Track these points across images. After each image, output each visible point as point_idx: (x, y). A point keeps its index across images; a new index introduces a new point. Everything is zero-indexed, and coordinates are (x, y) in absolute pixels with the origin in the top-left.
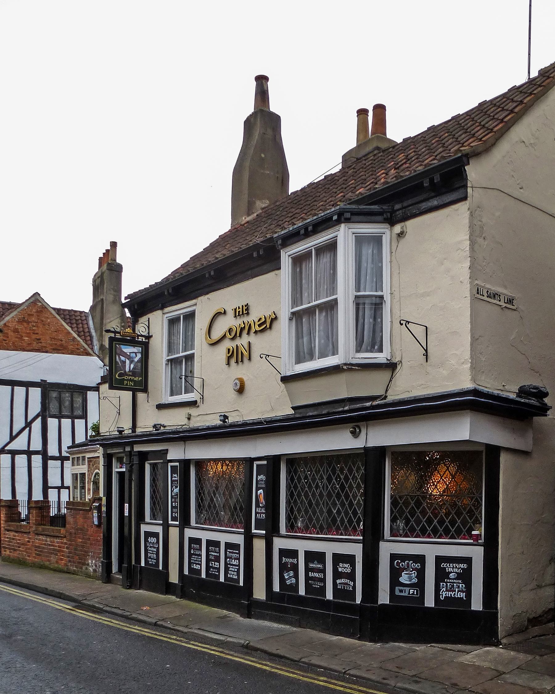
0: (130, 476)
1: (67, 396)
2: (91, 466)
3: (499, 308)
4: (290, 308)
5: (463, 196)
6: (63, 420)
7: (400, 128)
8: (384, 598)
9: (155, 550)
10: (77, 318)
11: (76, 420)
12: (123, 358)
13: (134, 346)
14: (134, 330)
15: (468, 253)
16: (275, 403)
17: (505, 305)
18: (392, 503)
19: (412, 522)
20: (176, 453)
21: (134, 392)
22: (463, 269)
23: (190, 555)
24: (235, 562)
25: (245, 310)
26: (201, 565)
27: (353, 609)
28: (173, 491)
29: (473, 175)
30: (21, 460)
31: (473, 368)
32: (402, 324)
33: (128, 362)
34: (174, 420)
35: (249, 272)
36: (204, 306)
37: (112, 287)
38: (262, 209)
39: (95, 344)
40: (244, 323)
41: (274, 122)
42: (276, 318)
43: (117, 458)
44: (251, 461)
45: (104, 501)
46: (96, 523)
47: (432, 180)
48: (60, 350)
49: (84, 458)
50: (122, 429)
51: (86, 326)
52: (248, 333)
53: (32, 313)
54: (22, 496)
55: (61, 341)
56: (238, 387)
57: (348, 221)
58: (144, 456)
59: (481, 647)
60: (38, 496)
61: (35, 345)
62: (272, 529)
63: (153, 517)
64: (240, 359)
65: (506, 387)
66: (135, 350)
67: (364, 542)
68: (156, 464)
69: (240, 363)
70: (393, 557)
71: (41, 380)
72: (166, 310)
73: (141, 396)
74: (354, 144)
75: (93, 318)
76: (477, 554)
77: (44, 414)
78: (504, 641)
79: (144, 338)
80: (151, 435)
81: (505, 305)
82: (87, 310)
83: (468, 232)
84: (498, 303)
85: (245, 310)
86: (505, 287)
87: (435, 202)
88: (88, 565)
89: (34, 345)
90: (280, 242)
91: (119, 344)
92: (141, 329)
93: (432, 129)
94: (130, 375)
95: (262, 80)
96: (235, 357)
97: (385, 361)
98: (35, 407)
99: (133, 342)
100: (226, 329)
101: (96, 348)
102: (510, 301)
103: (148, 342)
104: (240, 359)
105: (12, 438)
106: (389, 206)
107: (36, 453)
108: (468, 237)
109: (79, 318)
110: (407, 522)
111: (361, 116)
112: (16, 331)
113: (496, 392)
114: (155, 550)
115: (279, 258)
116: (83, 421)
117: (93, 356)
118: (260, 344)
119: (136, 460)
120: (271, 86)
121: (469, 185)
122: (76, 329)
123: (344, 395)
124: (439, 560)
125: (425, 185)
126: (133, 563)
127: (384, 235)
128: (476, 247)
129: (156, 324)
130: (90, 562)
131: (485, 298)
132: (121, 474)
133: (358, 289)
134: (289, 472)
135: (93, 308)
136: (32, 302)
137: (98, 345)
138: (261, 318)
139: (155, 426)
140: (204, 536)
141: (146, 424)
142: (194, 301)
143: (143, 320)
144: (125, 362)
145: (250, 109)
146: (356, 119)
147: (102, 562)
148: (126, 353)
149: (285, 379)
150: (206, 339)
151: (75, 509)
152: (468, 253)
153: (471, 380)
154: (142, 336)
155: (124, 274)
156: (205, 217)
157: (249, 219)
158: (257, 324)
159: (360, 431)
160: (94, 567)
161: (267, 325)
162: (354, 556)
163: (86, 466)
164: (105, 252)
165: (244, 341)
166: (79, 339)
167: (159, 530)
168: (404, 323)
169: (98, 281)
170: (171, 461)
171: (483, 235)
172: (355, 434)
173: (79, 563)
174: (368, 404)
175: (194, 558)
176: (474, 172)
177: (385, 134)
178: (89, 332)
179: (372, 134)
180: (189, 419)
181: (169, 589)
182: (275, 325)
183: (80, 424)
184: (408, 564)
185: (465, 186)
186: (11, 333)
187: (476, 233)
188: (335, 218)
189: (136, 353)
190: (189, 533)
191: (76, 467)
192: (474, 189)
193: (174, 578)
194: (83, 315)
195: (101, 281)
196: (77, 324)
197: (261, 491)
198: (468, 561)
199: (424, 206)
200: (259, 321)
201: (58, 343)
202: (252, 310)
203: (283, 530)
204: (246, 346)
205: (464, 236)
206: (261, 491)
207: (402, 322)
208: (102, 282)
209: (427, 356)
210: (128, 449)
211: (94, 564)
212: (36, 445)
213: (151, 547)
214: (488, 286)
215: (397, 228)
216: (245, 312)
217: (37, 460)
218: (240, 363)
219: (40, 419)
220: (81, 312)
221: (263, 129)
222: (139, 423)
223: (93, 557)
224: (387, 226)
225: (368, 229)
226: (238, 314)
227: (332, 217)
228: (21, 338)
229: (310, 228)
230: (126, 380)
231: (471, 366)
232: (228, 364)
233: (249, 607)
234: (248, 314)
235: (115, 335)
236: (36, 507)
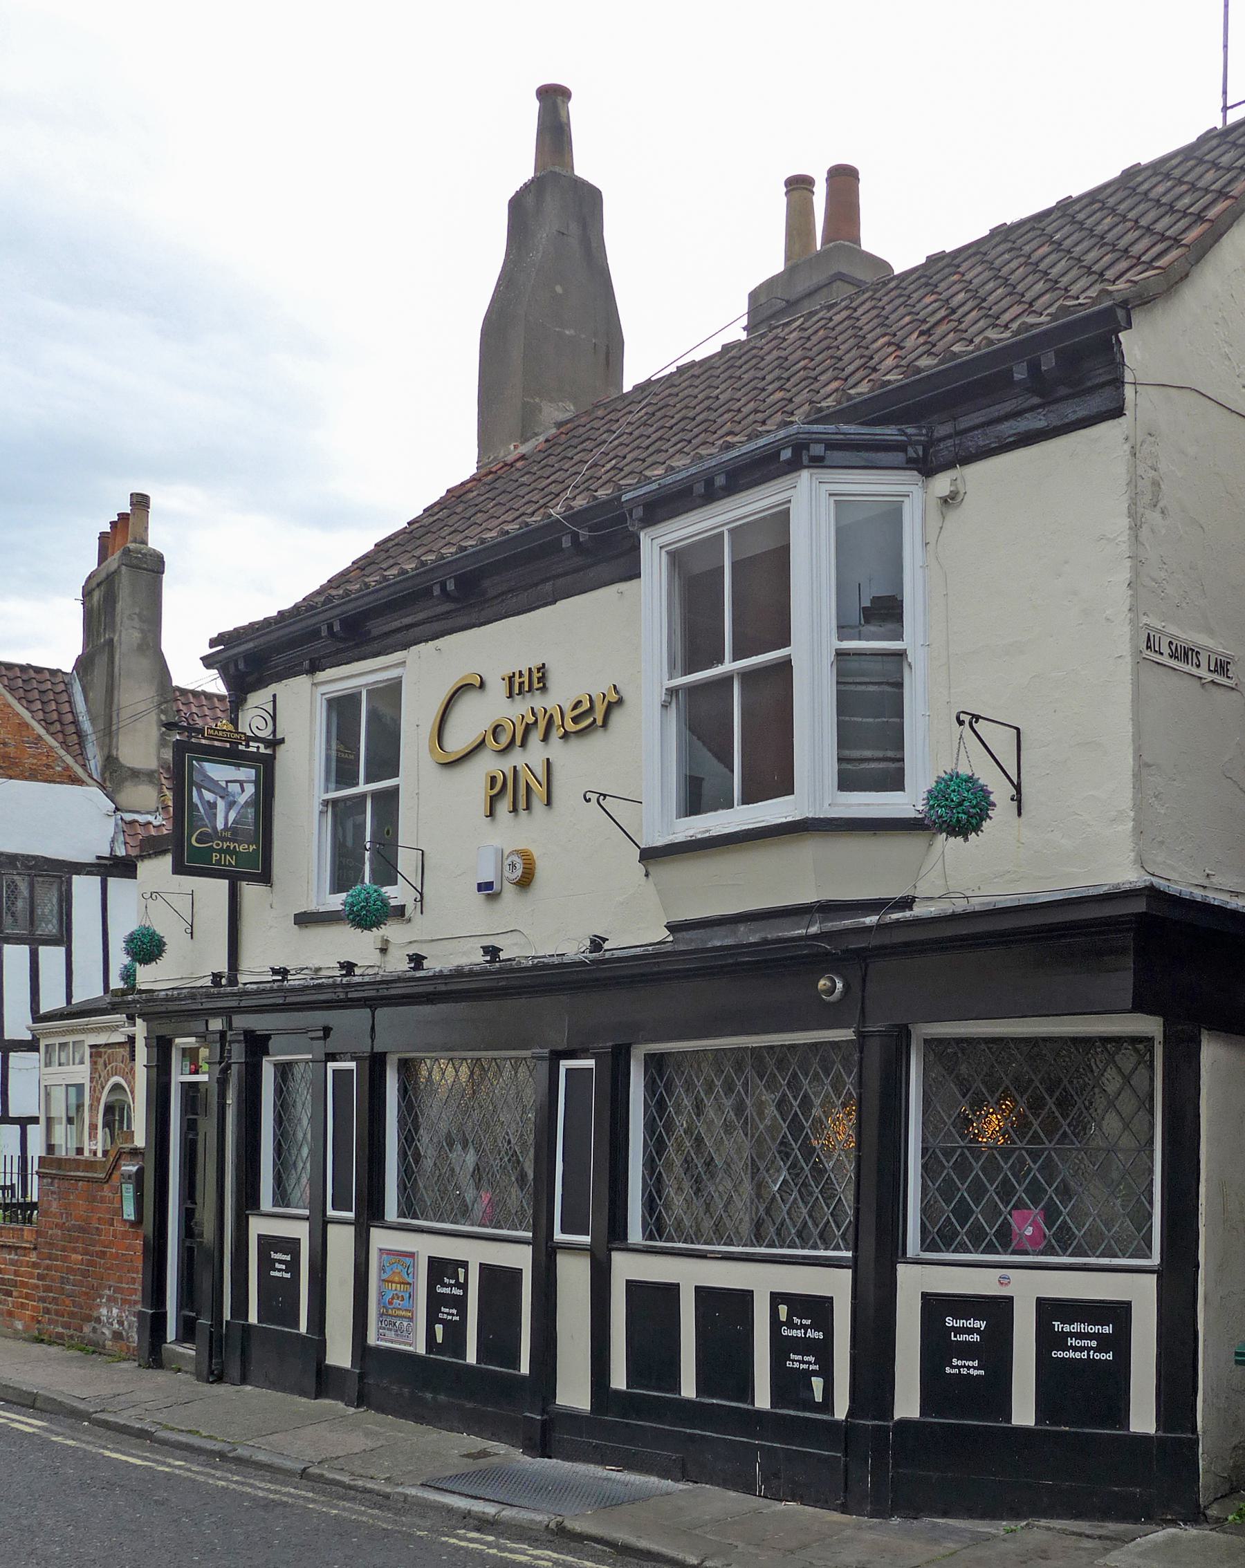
2: (100, 1067)
3: (1197, 683)
4: (666, 676)
5: (1113, 405)
7: (902, 233)
8: (907, 1404)
11: (42, 949)
12: (208, 796)
13: (238, 766)
14: (234, 722)
15: (1125, 548)
17: (1210, 677)
18: (925, 1167)
19: (978, 1215)
21: (234, 881)
22: (1113, 586)
25: (538, 680)
29: (1137, 353)
31: (1139, 831)
32: (961, 723)
33: (221, 805)
35: (548, 587)
36: (423, 672)
37: (137, 610)
38: (559, 425)
39: (90, 756)
40: (534, 714)
41: (587, 202)
42: (620, 702)
47: (1034, 367)
52: (545, 738)
56: (519, 872)
57: (817, 462)
59: (1154, 1527)
62: (370, 1212)
63: (281, 1196)
64: (522, 803)
65: (1214, 880)
67: (855, 1265)
69: (523, 813)
73: (250, 891)
74: (777, 265)
76: (1141, 1294)
78: (1213, 1512)
79: (261, 746)
81: (1210, 677)
82: (68, 667)
83: (1126, 497)
84: (1195, 671)
85: (538, 680)
86: (1211, 632)
87: (1036, 422)
88: (98, 1320)
90: (638, 512)
92: (253, 720)
93: (1002, 234)
94: (224, 839)
95: (553, 100)
99: (232, 755)
100: (488, 725)
101: (95, 764)
102: (1222, 667)
103: (273, 757)
104: (522, 803)
106: (919, 428)
110: (1050, 1215)
111: (796, 194)
113: (1198, 894)
115: (636, 548)
116: (61, 951)
118: (577, 765)
119: (237, 1053)
120: (578, 114)
121: (1128, 377)
122: (40, 715)
123: (808, 896)
124: (1048, 1309)
125: (1017, 377)
126: (227, 1315)
127: (906, 500)
128: (1144, 533)
129: (297, 711)
131: (1165, 660)
134: (650, 1087)
135: (83, 664)
137: (98, 757)
138: (580, 702)
140: (689, 1276)
141: (256, 967)
142: (398, 656)
143: (258, 699)
144: (213, 806)
145: (525, 171)
146: (783, 200)
147: (140, 1315)
148: (216, 783)
149: (649, 856)
150: (431, 750)
151: (64, 1178)
152: (1124, 547)
153: (1135, 862)
154: (257, 739)
155: (166, 578)
156: (404, 441)
157: (523, 449)
158: (569, 715)
160: (116, 1326)
161: (594, 717)
162: (750, 1293)
163: (86, 1068)
164: (116, 519)
165: (534, 755)
167: (300, 1231)
168: (966, 718)
171: (1161, 504)
173: (72, 1315)
174: (871, 920)
176: (1135, 346)
177: (857, 240)
178: (75, 722)
179: (825, 240)
180: (383, 951)
181: (324, 1381)
182: (617, 717)
183: (52, 957)
185: (1119, 382)
187: (1145, 498)
188: (786, 454)
189: (241, 783)
191: (55, 1068)
192: (1139, 388)
193: (339, 1354)
198: (1119, 1313)
199: (1009, 429)
200: (575, 708)
202: (553, 681)
203: (635, 1234)
204: (541, 772)
207: (963, 717)
208: (110, 599)
209: (1019, 801)
210: (216, 1024)
211: (117, 1316)
214: (1172, 630)
215: (942, 483)
216: (536, 685)
218: (523, 813)
220: (54, 673)
221: (556, 224)
222: (246, 963)
225: (870, 484)
226: (516, 686)
227: (778, 454)
229: (720, 481)
230: (216, 851)
231: (1134, 828)
232: (491, 814)
233: (546, 1427)
234: (544, 689)
235: (190, 737)
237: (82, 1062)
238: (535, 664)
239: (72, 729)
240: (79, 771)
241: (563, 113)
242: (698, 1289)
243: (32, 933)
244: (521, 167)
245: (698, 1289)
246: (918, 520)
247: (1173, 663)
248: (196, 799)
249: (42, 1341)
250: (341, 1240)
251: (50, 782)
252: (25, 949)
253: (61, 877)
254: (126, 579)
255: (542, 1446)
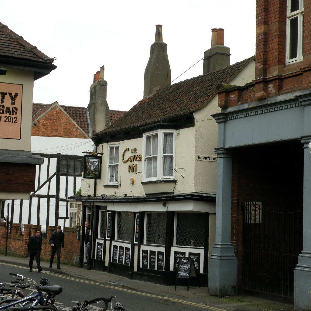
0: (93, 217)
1: (72, 163)
6: (69, 177)
9: (101, 251)
10: (80, 113)
12: (90, 164)
13: (95, 159)
16: (139, 191)
20: (110, 208)
22: (193, 150)
23: (113, 253)
24: (128, 256)
25: (134, 151)
26: (117, 257)
27: (155, 272)
28: (108, 224)
30: (44, 201)
33: (92, 165)
34: (110, 193)
36: (124, 145)
38: (157, 91)
39: (90, 130)
43: (88, 207)
44: (135, 213)
45: (81, 228)
46: (78, 238)
48: (68, 135)
49: (76, 204)
50: (89, 195)
51: (85, 118)
53: (53, 114)
54: (43, 223)
55: (70, 130)
58: (99, 208)
60: (52, 223)
61: (54, 133)
62: (112, 239)
66: (96, 160)
68: (103, 211)
70: (175, 253)
71: (57, 153)
72: (109, 143)
73: (98, 181)
75: (89, 113)
76: (202, 252)
77: (58, 174)
80: (100, 199)
82: (86, 107)
84: (210, 160)
88: (73, 259)
89: (54, 133)
91: (89, 158)
94: (93, 172)
95: (159, 27)
96: (132, 169)
97: (172, 180)
98: (53, 169)
103: (102, 157)
105: (39, 188)
107: (53, 197)
108: (194, 139)
109: (81, 112)
112: (44, 125)
114: (101, 251)
117: (88, 138)
121: (195, 121)
126: (92, 258)
130: (74, 258)
131: (202, 160)
132: (89, 215)
133: (164, 153)
135: (89, 106)
136: (53, 108)
139: (102, 195)
140: (119, 244)
143: (100, 146)
147: (79, 258)
149: (143, 183)
151: (69, 232)
159: (166, 204)
160: (76, 260)
163: (77, 208)
165: (134, 163)
166: (80, 128)
167: (102, 242)
169: (93, 90)
170: (108, 211)
172: (164, 206)
175: (115, 254)
176: (197, 117)
178: (87, 121)
180: (115, 193)
181: (104, 269)
184: (180, 255)
186: (41, 126)
189: (96, 162)
190: (114, 243)
193: (107, 264)
194: (84, 110)
195: (94, 91)
196: (80, 117)
197: (138, 226)
201: (68, 131)
205: (193, 139)
206: (138, 226)
208: (95, 91)
212: (53, 192)
213: (99, 250)
215: (178, 131)
217: (53, 201)
219: (55, 177)
221: (159, 50)
223: (75, 256)
224: (175, 130)
228: (47, 129)
234: (136, 152)
236: (50, 230)
237: (76, 207)
238: (135, 148)
239: (86, 123)
240: (86, 135)
241: (160, 30)
242: (150, 251)
243: (74, 173)
244: (152, 40)
245: (150, 251)
246: (175, 136)
247: (204, 160)
248: (88, 165)
249: (64, 264)
250: (108, 243)
251: (79, 138)
252: (73, 178)
253: (81, 160)
254: (99, 88)
255: (131, 278)
